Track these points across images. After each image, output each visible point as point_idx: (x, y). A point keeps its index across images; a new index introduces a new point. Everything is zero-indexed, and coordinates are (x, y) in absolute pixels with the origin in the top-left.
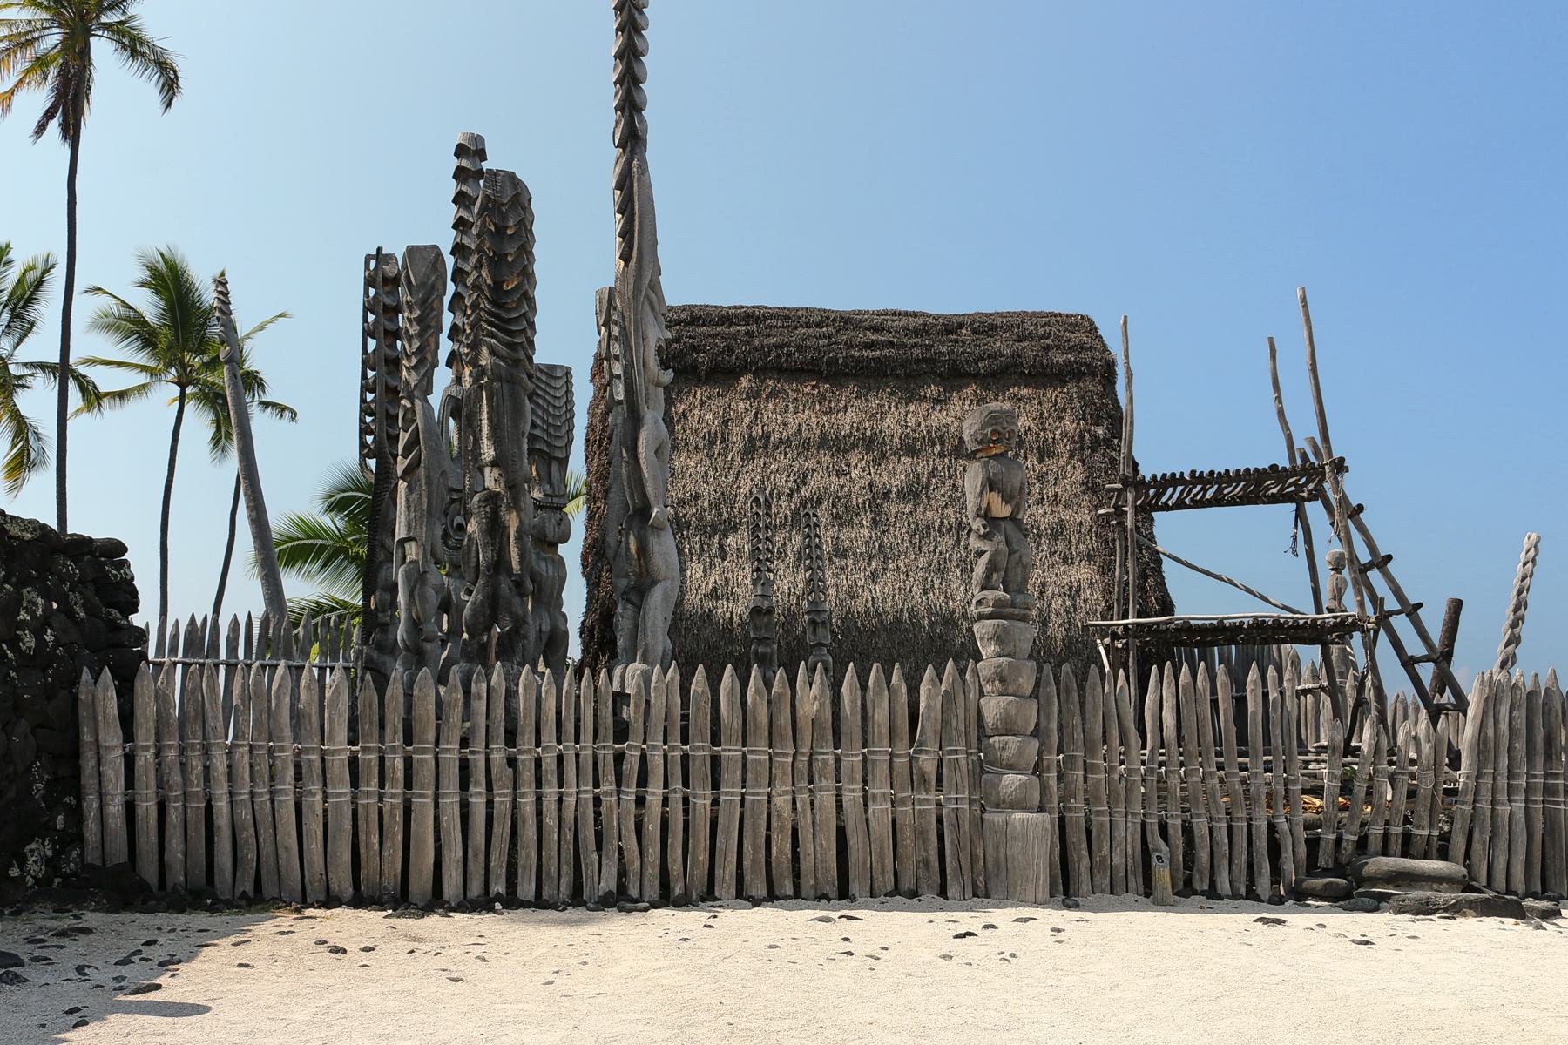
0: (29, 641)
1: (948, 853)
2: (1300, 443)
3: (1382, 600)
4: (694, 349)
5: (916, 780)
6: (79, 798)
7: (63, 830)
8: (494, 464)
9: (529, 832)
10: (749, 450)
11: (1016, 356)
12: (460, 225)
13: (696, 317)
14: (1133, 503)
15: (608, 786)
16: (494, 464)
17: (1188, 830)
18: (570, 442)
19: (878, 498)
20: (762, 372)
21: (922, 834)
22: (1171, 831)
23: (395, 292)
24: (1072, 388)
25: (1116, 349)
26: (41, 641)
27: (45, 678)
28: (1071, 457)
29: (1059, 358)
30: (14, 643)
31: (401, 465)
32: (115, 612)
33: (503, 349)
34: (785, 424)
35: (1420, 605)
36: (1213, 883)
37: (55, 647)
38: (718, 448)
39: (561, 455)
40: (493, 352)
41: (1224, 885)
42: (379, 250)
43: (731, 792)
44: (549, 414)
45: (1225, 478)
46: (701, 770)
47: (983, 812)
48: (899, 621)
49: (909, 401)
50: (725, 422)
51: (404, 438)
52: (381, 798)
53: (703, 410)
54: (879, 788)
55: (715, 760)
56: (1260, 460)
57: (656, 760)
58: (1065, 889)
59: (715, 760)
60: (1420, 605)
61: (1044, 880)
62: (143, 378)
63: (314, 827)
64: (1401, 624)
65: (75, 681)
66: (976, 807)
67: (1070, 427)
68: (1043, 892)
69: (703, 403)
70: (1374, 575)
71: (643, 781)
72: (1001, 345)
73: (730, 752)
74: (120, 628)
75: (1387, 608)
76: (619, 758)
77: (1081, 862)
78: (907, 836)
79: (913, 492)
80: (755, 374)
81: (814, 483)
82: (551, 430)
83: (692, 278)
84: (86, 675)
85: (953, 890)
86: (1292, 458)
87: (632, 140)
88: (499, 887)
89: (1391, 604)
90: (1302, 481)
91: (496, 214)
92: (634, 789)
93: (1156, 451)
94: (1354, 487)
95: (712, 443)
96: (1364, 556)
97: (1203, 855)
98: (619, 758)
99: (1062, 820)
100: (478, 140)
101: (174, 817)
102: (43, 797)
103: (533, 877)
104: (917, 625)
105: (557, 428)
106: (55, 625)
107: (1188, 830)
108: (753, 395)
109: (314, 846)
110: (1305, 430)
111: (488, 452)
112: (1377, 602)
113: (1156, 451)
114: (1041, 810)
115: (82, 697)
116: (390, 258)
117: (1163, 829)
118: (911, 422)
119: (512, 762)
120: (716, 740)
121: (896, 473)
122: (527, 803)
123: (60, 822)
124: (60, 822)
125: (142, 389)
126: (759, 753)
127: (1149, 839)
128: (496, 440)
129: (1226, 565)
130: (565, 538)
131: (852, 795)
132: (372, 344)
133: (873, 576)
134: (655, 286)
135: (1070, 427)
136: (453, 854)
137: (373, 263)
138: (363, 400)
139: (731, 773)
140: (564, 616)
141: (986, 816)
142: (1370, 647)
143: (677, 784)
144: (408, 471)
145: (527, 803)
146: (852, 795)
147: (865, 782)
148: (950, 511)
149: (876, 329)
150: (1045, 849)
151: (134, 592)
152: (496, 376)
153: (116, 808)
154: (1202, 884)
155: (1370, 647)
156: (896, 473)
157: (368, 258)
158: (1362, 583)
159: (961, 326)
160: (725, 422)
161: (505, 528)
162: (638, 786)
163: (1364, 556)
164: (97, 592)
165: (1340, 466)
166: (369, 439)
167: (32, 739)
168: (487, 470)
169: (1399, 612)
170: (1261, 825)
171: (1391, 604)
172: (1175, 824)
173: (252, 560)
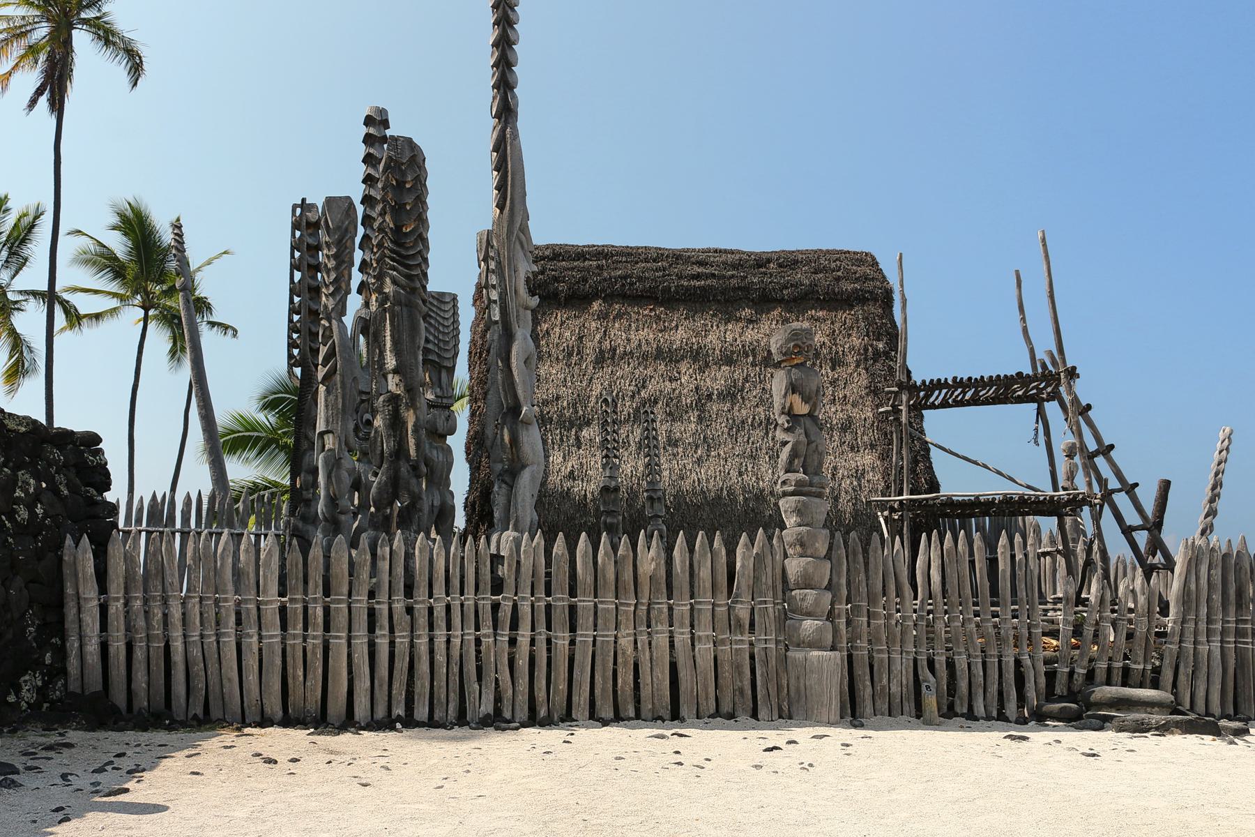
0: (23, 514)
1: (759, 683)
2: (1041, 355)
3: (1106, 480)
4: (556, 279)
5: (733, 624)
6: (64, 640)
7: (51, 665)
8: (395, 371)
9: (423, 667)
10: (600, 361)
11: (813, 285)
12: (368, 180)
13: (557, 254)
14: (907, 403)
15: (486, 630)
16: (395, 371)
17: (951, 665)
18: (456, 354)
19: (703, 399)
20: (610, 298)
21: (738, 668)
22: (937, 666)
23: (316, 234)
24: (858, 311)
25: (893, 279)
26: (32, 514)
27: (36, 543)
28: (858, 366)
29: (848, 286)
30: (11, 515)
31: (321, 372)
32: (92, 490)
33: (402, 280)
34: (629, 340)
35: (1137, 485)
36: (970, 708)
37: (44, 518)
38: (575, 358)
39: (449, 365)
40: (394, 282)
41: (980, 709)
42: (304, 200)
43: (585, 634)
44: (440, 332)
45: (980, 383)
46: (561, 616)
47: (787, 650)
48: (719, 497)
49: (728, 321)
50: (581, 338)
51: (323, 351)
52: (305, 639)
53: (563, 328)
54: (704, 631)
55: (573, 609)
56: (1008, 369)
57: (525, 608)
58: (853, 712)
59: (573, 609)
60: (1137, 485)
61: (835, 705)
62: (114, 303)
63: (251, 662)
64: (1121, 500)
65: (60, 545)
66: (782, 646)
67: (856, 342)
68: (835, 715)
69: (562, 323)
70: (1100, 461)
71: (514, 625)
72: (802, 276)
73: (585, 602)
74: (96, 503)
75: (1110, 487)
76: (496, 607)
77: (865, 691)
78: (726, 669)
79: (731, 394)
80: (604, 300)
81: (652, 387)
82: (441, 345)
83: (554, 223)
84: (69, 541)
85: (762, 713)
86: (1034, 367)
87: (506, 112)
88: (399, 711)
89: (1114, 484)
90: (1042, 385)
91: (397, 171)
92: (507, 632)
93: (925, 361)
94: (1084, 390)
95: (570, 355)
96: (1092, 446)
97: (963, 685)
98: (496, 607)
99: (850, 657)
100: (383, 112)
101: (139, 654)
102: (34, 638)
103: (427, 703)
104: (734, 500)
105: (446, 343)
106: (44, 501)
107: (951, 665)
108: (603, 316)
109: (252, 678)
110: (1044, 344)
111: (391, 362)
112: (1102, 482)
113: (925, 361)
114: (833, 648)
115: (66, 558)
116: (312, 207)
117: (931, 664)
118: (729, 338)
119: (410, 610)
120: (573, 593)
121: (717, 379)
122: (422, 643)
123: (48, 658)
124: (48, 658)
125: (114, 311)
126: (608, 603)
127: (920, 672)
128: (397, 352)
129: (982, 453)
130: (452, 431)
131: (682, 637)
132: (298, 276)
133: (699, 461)
134: (524, 229)
135: (856, 342)
136: (363, 684)
137: (298, 211)
138: (291, 321)
139: (585, 619)
140: (452, 493)
141: (789, 654)
142: (1097, 518)
143: (542, 628)
144: (327, 378)
145: (422, 643)
146: (682, 637)
147: (692, 626)
148: (761, 409)
149: (701, 263)
150: (836, 680)
151: (107, 475)
152: (397, 301)
153: (93, 647)
154: (962, 708)
155: (1097, 518)
156: (717, 379)
157: (295, 207)
158: (1090, 467)
159: (769, 261)
160: (581, 338)
161: (404, 423)
162: (511, 629)
163: (1092, 446)
164: (78, 474)
165: (1072, 373)
166: (296, 352)
167: (25, 592)
168: (390, 376)
169: (1119, 491)
170: (1010, 661)
171: (1114, 484)
172: (941, 660)
173: (201, 448)
